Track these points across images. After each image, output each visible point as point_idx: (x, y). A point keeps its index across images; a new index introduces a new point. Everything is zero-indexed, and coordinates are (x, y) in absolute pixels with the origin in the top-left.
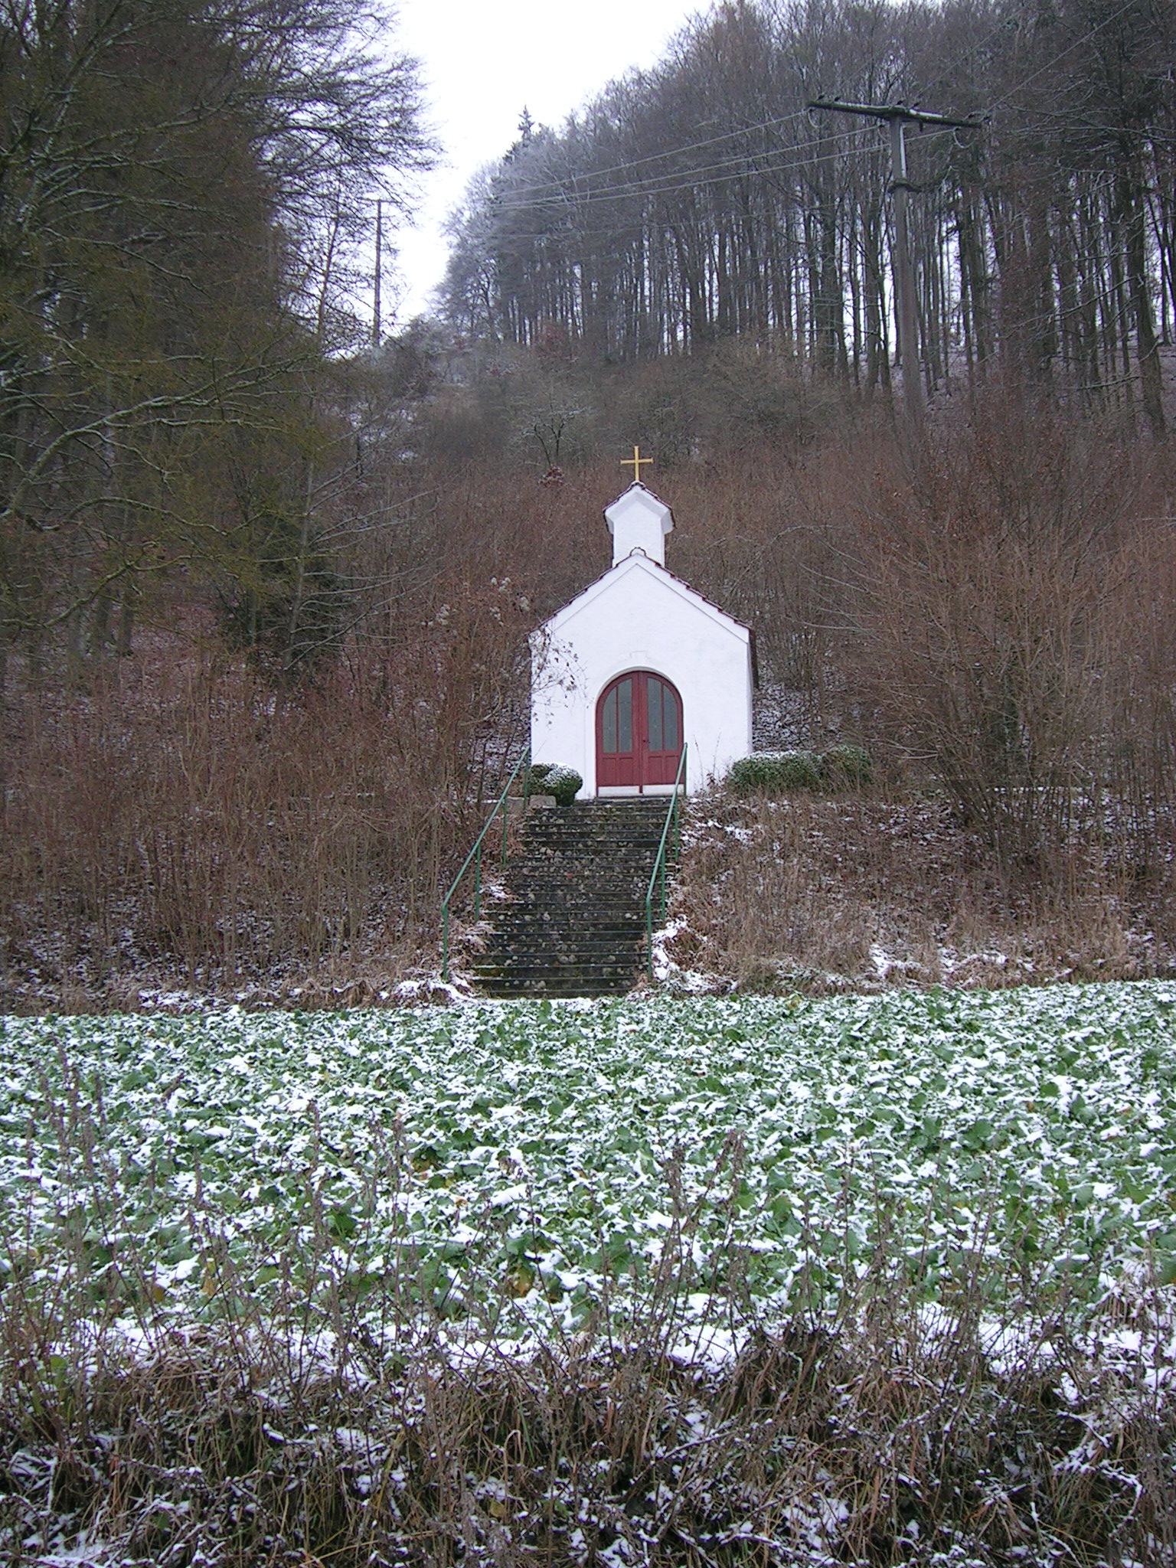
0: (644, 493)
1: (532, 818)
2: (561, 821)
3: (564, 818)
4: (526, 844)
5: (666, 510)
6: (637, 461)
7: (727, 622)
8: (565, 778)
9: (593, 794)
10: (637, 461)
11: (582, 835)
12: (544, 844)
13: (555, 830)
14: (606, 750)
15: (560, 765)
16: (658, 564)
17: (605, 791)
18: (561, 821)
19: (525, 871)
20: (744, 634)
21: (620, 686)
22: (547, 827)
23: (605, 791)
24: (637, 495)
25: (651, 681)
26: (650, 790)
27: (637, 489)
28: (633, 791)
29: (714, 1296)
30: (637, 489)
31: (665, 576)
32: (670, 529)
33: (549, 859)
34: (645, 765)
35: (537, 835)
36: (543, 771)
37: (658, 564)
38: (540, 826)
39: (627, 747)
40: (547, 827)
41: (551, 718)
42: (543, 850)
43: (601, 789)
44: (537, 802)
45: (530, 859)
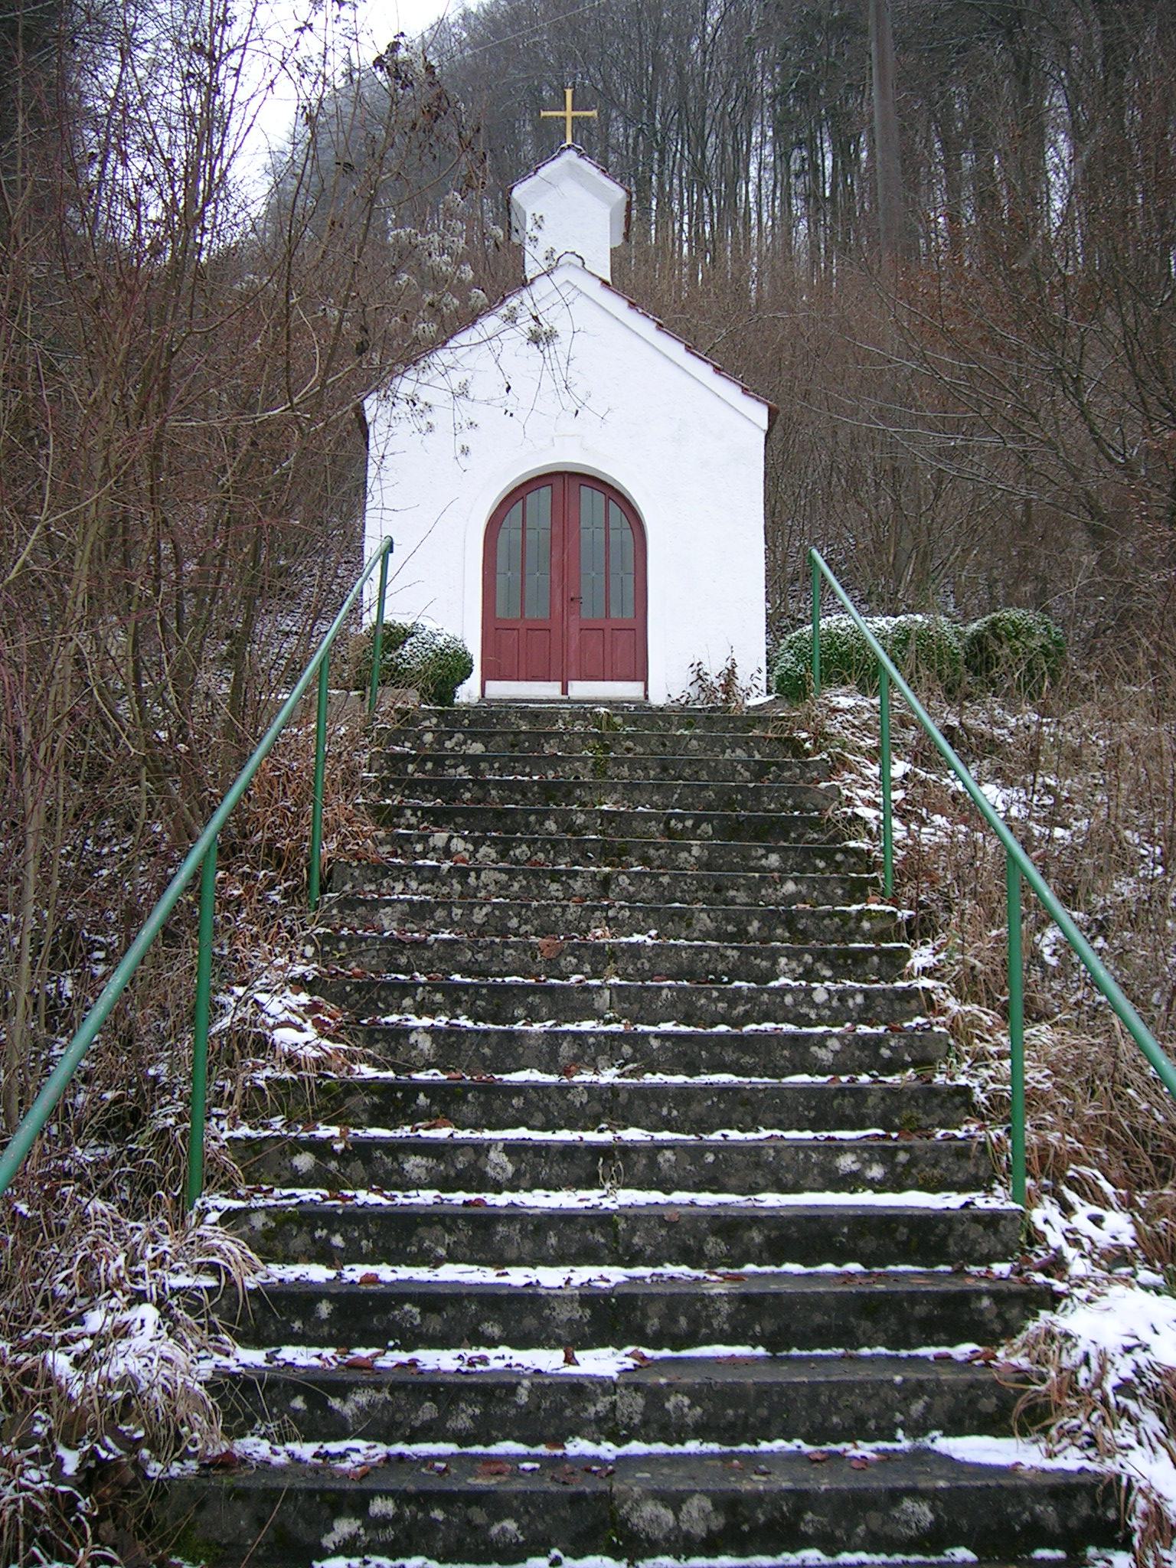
0: (581, 162)
1: (395, 738)
2: (477, 748)
3: (485, 738)
4: (385, 817)
5: (619, 194)
6: (569, 113)
7: (731, 391)
8: (441, 653)
10: (569, 113)
11: (549, 791)
12: (439, 818)
13: (462, 772)
15: (431, 626)
16: (605, 283)
17: (500, 689)
18: (477, 748)
19: (388, 922)
20: (759, 414)
22: (439, 761)
23: (500, 689)
24: (573, 172)
25: (586, 492)
26: (580, 689)
27: (570, 155)
28: (550, 690)
30: (570, 155)
31: (618, 305)
32: (619, 241)
33: (462, 874)
34: (574, 644)
35: (412, 787)
36: (393, 637)
37: (605, 283)
38: (420, 760)
39: (538, 611)
40: (439, 761)
41: (467, 438)
42: (439, 838)
43: (488, 683)
44: (390, 699)
45: (401, 873)
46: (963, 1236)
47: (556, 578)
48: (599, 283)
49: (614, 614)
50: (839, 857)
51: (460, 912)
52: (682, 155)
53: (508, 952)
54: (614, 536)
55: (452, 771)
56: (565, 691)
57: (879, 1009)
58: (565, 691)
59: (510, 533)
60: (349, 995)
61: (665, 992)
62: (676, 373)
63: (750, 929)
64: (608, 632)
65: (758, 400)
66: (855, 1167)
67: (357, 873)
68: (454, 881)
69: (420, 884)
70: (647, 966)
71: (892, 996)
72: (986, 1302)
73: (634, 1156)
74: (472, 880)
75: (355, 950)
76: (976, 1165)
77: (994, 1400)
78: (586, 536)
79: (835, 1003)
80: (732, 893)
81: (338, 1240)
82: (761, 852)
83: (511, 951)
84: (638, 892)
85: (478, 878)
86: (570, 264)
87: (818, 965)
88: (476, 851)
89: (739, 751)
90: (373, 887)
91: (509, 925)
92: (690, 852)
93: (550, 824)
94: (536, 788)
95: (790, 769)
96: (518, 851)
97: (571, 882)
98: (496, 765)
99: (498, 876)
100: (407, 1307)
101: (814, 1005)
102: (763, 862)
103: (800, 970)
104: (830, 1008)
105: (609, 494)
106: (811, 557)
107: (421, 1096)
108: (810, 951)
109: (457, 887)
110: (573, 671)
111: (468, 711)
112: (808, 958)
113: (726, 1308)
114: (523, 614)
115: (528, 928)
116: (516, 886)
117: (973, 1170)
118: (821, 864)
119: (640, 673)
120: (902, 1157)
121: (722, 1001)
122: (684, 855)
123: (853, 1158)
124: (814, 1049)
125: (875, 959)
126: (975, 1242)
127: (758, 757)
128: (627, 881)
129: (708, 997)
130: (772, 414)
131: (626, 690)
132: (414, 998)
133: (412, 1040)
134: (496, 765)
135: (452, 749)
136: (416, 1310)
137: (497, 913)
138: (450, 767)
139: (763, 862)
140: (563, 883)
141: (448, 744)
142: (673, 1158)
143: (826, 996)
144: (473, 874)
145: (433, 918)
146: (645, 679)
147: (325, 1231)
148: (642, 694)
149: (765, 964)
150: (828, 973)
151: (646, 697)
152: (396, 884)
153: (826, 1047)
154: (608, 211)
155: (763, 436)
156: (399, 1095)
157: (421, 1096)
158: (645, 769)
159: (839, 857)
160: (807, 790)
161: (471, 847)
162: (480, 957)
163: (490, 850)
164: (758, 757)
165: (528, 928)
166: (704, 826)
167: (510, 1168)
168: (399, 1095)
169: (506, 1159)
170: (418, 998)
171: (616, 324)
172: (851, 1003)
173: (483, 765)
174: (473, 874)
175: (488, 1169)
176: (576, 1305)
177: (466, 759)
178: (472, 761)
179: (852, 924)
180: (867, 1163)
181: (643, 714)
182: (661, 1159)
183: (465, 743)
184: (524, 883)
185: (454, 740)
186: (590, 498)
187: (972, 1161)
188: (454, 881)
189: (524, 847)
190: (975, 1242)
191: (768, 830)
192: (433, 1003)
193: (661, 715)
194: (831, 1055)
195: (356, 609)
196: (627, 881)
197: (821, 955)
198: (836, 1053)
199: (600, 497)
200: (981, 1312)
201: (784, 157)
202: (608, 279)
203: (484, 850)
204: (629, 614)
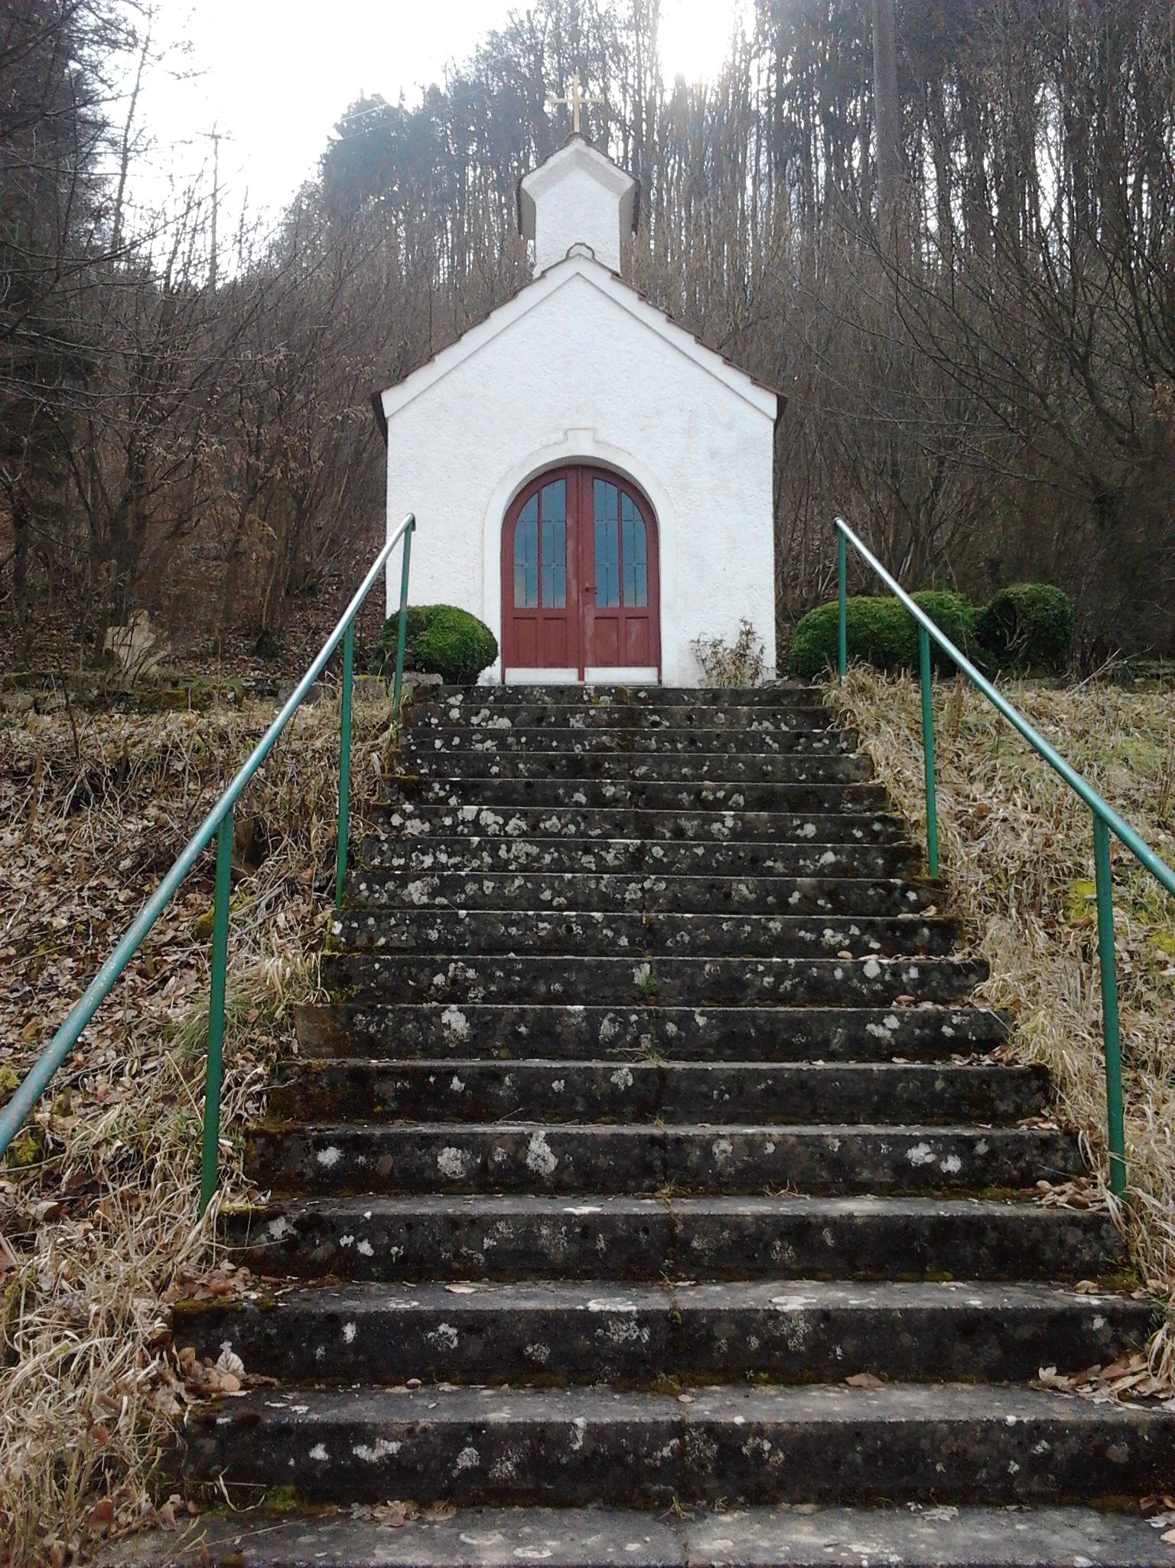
2: (504, 723)
7: (739, 381)
18: (504, 723)
20: (769, 404)
23: (519, 676)
25: (599, 484)
26: (598, 675)
31: (628, 298)
39: (555, 601)
46: (1062, 1242)
47: (571, 568)
48: (610, 274)
49: (626, 605)
50: (877, 827)
51: (492, 884)
52: (680, 167)
53: (541, 925)
54: (628, 532)
55: (479, 746)
56: (581, 677)
57: (934, 984)
58: (581, 677)
59: (526, 527)
60: (378, 972)
61: (707, 967)
62: (683, 363)
63: (791, 900)
64: (622, 621)
66: (930, 1159)
67: (385, 847)
68: (485, 854)
69: (450, 857)
70: (687, 938)
71: (949, 970)
72: (1099, 1323)
73: (687, 1147)
74: (503, 853)
75: (383, 925)
76: (1065, 1159)
77: (1126, 1447)
78: (599, 531)
79: (887, 977)
80: (769, 863)
81: (365, 1248)
82: (796, 822)
83: (546, 925)
84: (673, 863)
85: (508, 851)
87: (866, 937)
88: (506, 824)
89: (766, 724)
90: (402, 861)
91: (542, 897)
92: (723, 823)
93: (580, 797)
94: (564, 762)
95: (820, 741)
96: (548, 824)
97: (603, 853)
98: (523, 740)
99: (528, 848)
100: (443, 1328)
101: (864, 979)
102: (799, 832)
103: (847, 942)
104: (883, 982)
105: (623, 487)
106: (836, 527)
107: (455, 1080)
108: (857, 924)
109: (488, 860)
110: (589, 660)
111: (489, 690)
112: (855, 930)
113: (803, 1327)
114: (540, 604)
115: (562, 900)
116: (548, 859)
117: (1061, 1164)
118: (859, 834)
119: (652, 656)
120: (982, 1148)
121: (768, 975)
122: (716, 826)
123: (927, 1149)
124: (870, 1027)
125: (926, 931)
126: (1074, 1249)
127: (785, 728)
128: (661, 853)
129: (754, 972)
130: (782, 404)
131: (639, 676)
132: (446, 974)
133: (445, 1020)
134: (523, 740)
135: (479, 725)
136: (452, 1331)
137: (529, 885)
138: (478, 742)
139: (799, 832)
140: (595, 855)
141: (474, 720)
142: (730, 1148)
143: (878, 970)
144: (503, 847)
145: (463, 891)
146: (658, 665)
147: (352, 1238)
149: (808, 936)
150: (875, 945)
151: (660, 681)
152: (425, 858)
153: (884, 1025)
154: (617, 201)
155: (771, 426)
156: (432, 1079)
157: (455, 1080)
158: (673, 742)
159: (877, 827)
160: (838, 761)
161: (501, 821)
162: (513, 930)
163: (520, 823)
164: (785, 728)
165: (562, 900)
166: (735, 797)
167: (553, 1162)
168: (432, 1079)
169: (548, 1149)
170: (450, 974)
172: (904, 977)
173: (510, 740)
174: (503, 847)
175: (529, 1161)
176: (632, 1324)
177: (493, 734)
178: (497, 735)
179: (897, 894)
180: (942, 1155)
181: (661, 696)
182: (716, 1150)
183: (491, 718)
184: (556, 855)
185: (481, 716)
186: (604, 493)
187: (1060, 1153)
188: (485, 854)
189: (554, 819)
190: (1074, 1249)
191: (802, 802)
192: (466, 979)
193: (676, 695)
194: (888, 1034)
195: (380, 585)
196: (661, 853)
197: (868, 927)
198: (894, 1031)
199: (613, 490)
200: (1094, 1334)
201: (779, 165)
202: (618, 270)
203: (513, 822)
204: (642, 602)
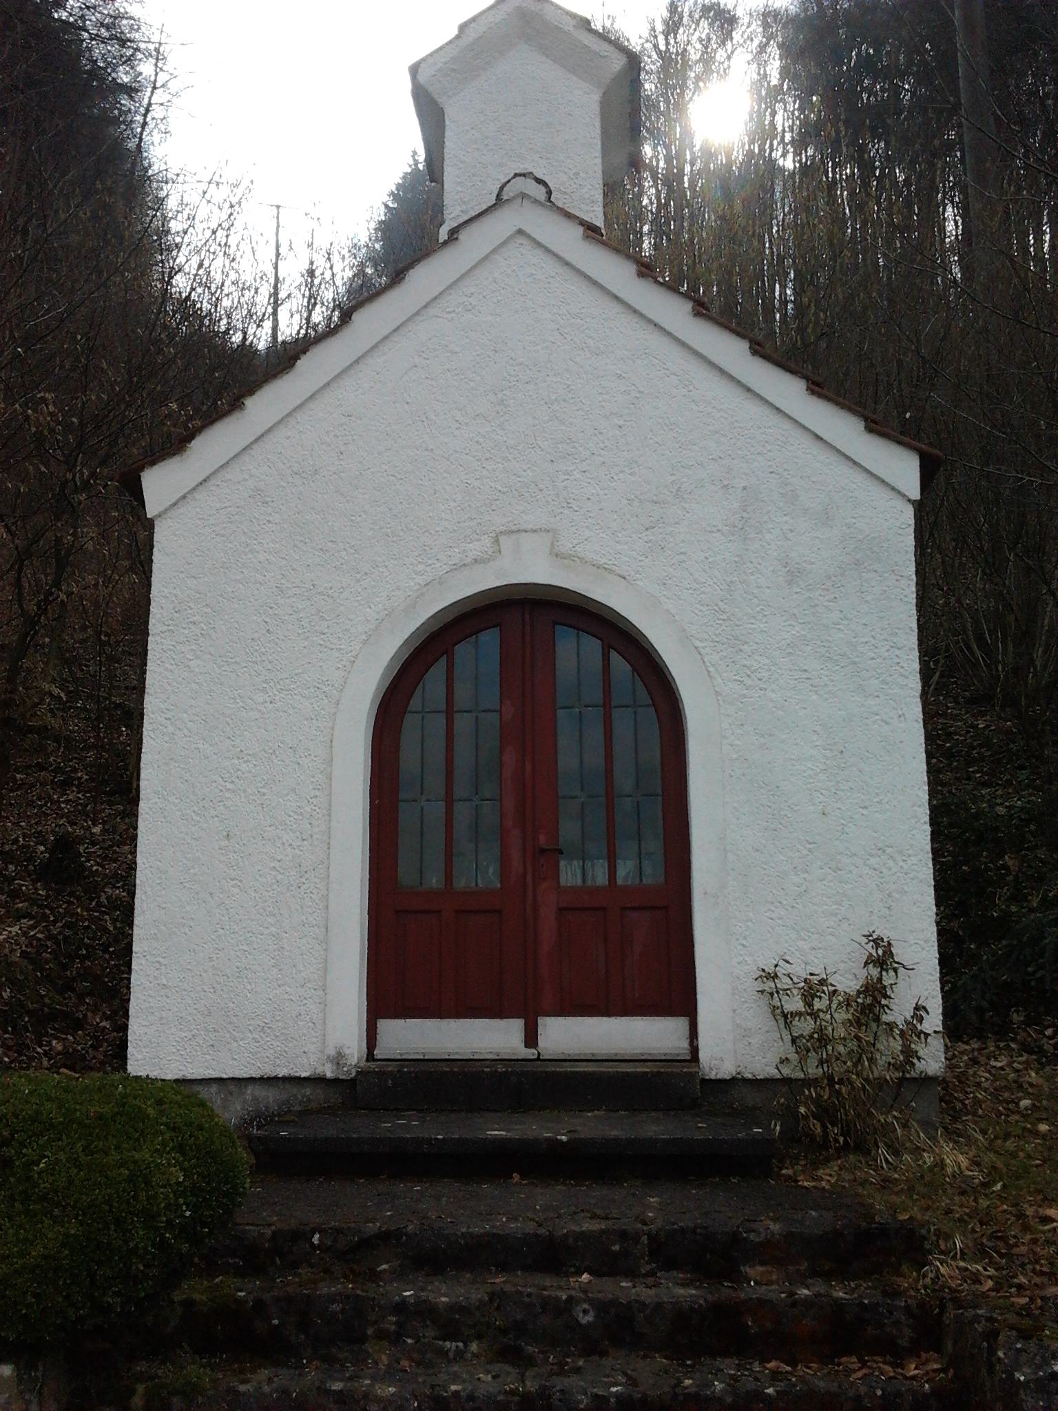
9: (355, 1050)
14: (406, 873)
16: (591, 230)
21: (463, 651)
29: (530, 1053)
37: (591, 230)
48: (581, 229)
56: (531, 1038)
58: (531, 1038)
65: (899, 443)
86: (524, 196)
148: (685, 1044)
151: (694, 1050)
154: (596, 97)
155: (908, 516)
171: (614, 309)
199: (592, 646)
202: (599, 222)
204: (653, 874)
